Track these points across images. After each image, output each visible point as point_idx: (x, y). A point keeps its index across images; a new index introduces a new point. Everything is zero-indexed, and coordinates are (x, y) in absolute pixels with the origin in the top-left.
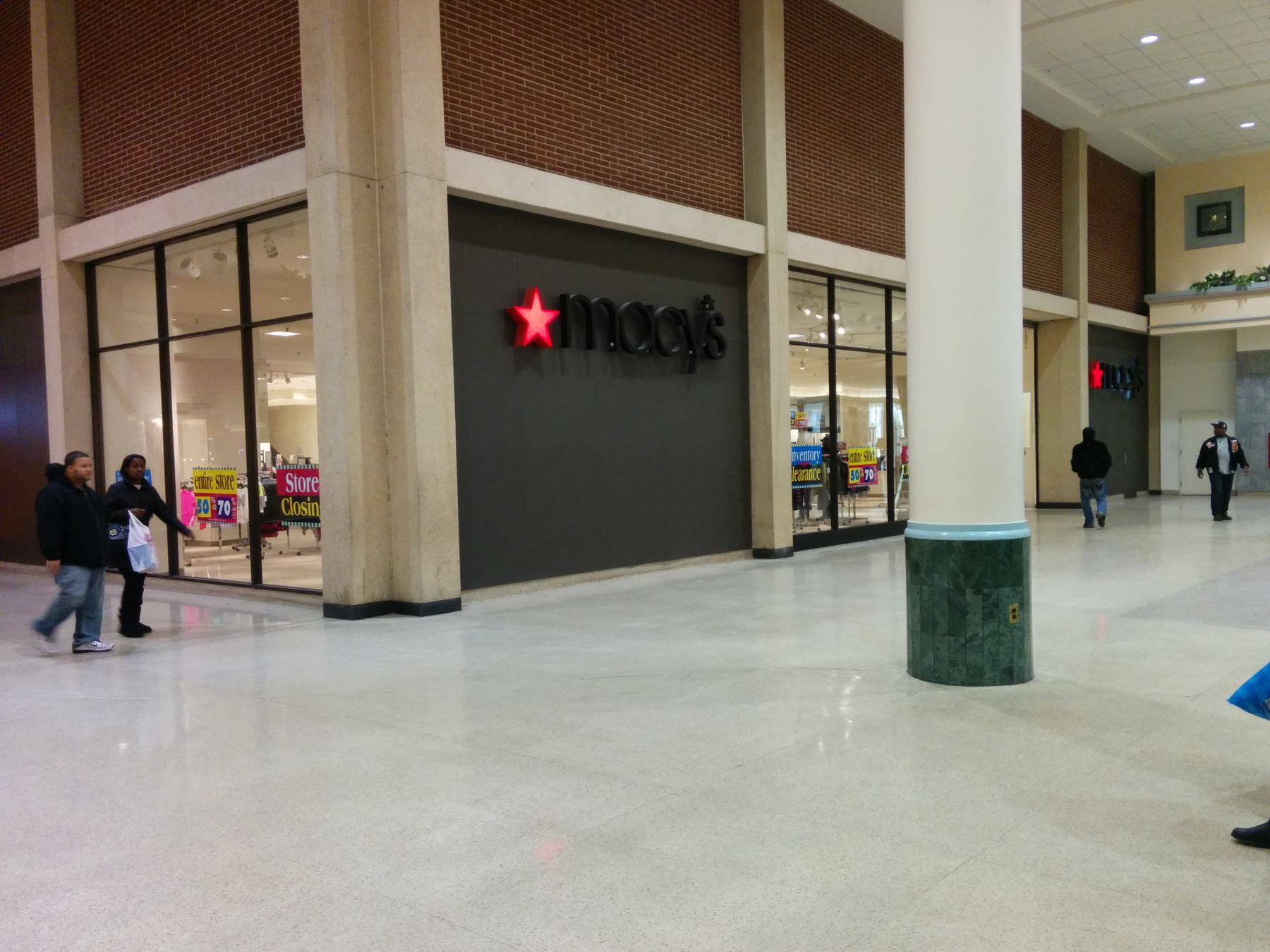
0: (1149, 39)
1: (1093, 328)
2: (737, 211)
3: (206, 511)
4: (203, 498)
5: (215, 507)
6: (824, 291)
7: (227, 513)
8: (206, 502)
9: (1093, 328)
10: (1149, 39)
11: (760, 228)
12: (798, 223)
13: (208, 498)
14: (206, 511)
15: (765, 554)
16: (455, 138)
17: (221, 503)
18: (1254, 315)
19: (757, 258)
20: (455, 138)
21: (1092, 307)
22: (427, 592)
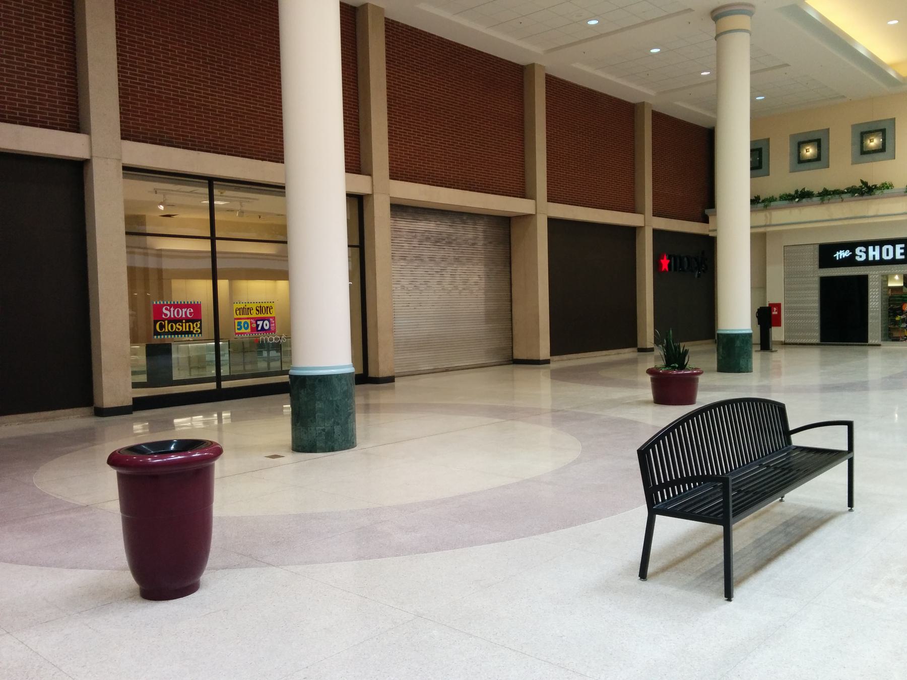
0: (593, 22)
1: (552, 221)
2: (523, 195)
3: (246, 329)
4: (243, 321)
5: (254, 325)
6: (206, 190)
7: (266, 328)
8: (246, 323)
9: (552, 221)
10: (593, 22)
11: (533, 201)
12: (552, 198)
13: (248, 321)
14: (246, 329)
15: (101, 412)
16: (126, 135)
17: (260, 323)
18: (815, 219)
19: (370, 196)
20: (126, 135)
21: (129, 145)
22: (542, 358)
